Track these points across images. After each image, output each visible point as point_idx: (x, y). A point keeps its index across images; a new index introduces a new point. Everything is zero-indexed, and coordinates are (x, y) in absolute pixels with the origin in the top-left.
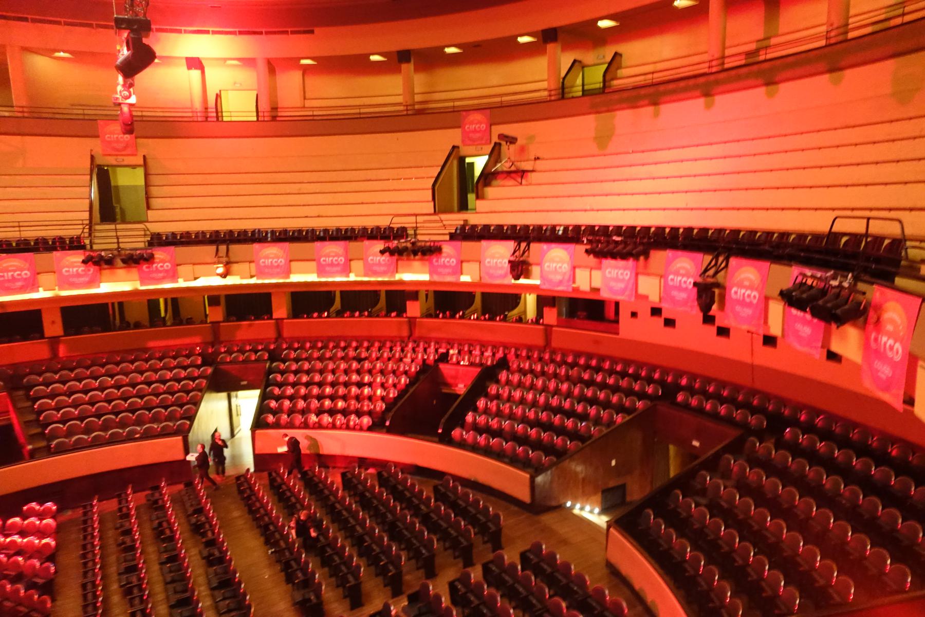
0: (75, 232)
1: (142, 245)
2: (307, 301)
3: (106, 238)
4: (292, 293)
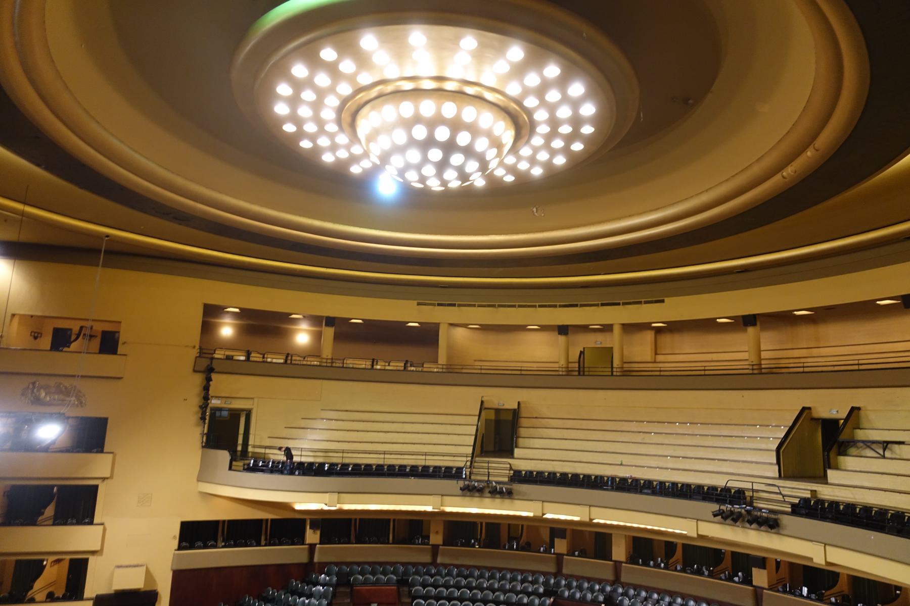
0: (460, 462)
1: (506, 479)
2: (644, 548)
3: (498, 469)
4: (634, 537)
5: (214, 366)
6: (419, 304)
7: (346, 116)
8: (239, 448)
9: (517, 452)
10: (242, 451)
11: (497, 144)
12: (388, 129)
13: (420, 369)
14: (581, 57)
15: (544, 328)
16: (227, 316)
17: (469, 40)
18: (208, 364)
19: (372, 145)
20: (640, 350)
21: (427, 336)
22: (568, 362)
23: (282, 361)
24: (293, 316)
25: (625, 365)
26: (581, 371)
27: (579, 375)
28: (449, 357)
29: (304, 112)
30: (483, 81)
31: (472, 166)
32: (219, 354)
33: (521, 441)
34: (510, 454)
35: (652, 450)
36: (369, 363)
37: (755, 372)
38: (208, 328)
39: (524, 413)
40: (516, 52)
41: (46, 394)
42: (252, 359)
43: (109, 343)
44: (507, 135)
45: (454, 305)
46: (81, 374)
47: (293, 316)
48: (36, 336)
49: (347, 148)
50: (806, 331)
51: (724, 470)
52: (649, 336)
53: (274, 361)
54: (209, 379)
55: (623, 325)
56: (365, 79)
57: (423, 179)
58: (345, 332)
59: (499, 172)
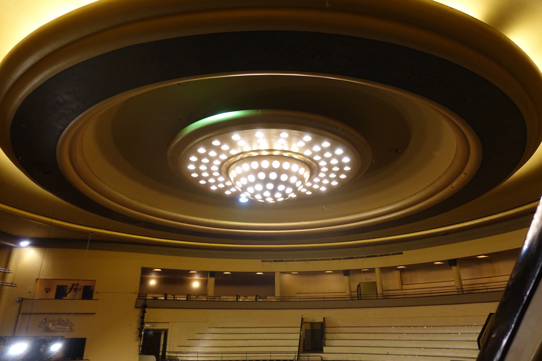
5: (147, 304)
6: (262, 261)
7: (223, 169)
8: (161, 354)
9: (325, 349)
10: (162, 356)
11: (301, 178)
12: (246, 175)
13: (265, 300)
14: (338, 137)
15: (335, 272)
16: (153, 273)
17: (285, 134)
18: (144, 302)
19: (237, 183)
20: (393, 283)
21: (268, 280)
22: (351, 292)
23: (185, 299)
24: (191, 272)
25: (385, 292)
26: (359, 297)
27: (358, 299)
28: (281, 292)
29: (203, 168)
30: (292, 150)
31: (289, 190)
32: (149, 297)
33: (327, 342)
34: (321, 351)
35: (405, 344)
36: (235, 298)
37: (460, 293)
38: (143, 281)
39: (327, 324)
40: (308, 138)
41: (52, 325)
42: (168, 298)
43: (88, 293)
44: (306, 175)
45: (282, 261)
46: (74, 312)
47: (191, 272)
48: (47, 291)
49: (224, 183)
50: (486, 267)
51: (449, 355)
52: (397, 274)
53: (181, 299)
54: (144, 312)
55: (380, 268)
56: (233, 152)
57: (264, 198)
58: (221, 280)
59: (304, 190)
